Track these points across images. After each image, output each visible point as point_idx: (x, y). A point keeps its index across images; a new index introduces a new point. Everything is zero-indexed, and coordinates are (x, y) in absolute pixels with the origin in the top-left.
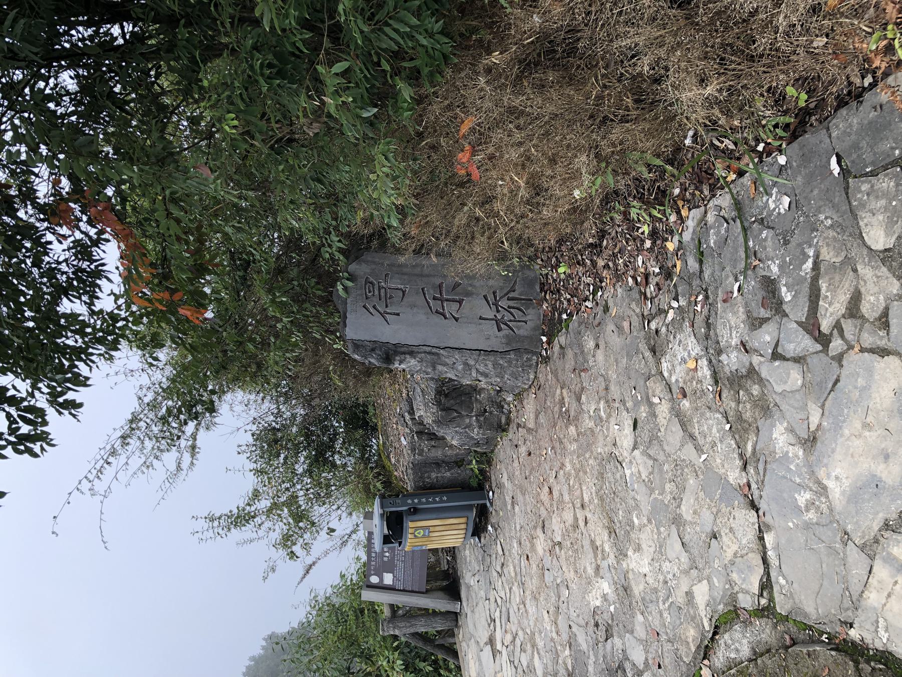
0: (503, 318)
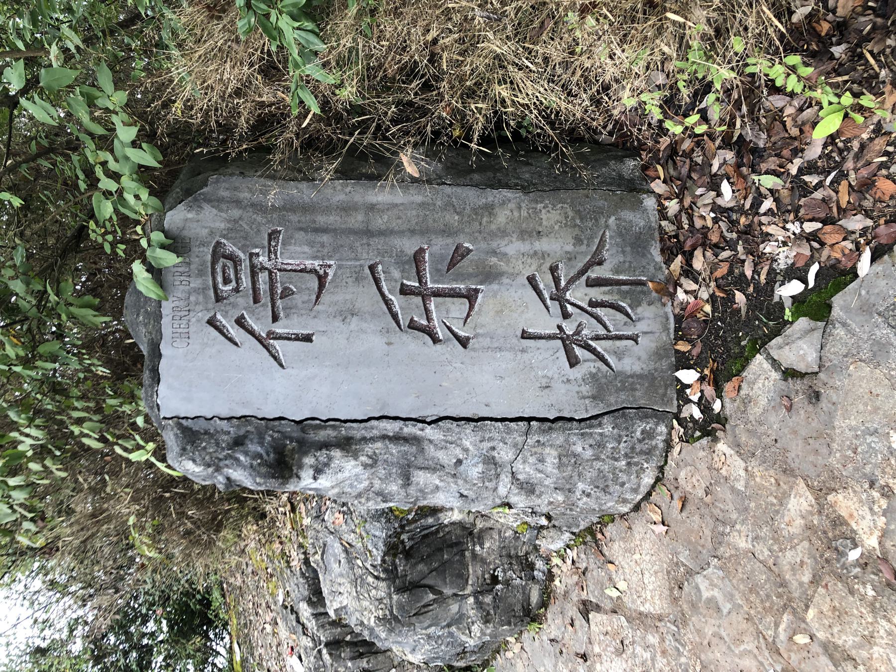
0: (578, 332)
